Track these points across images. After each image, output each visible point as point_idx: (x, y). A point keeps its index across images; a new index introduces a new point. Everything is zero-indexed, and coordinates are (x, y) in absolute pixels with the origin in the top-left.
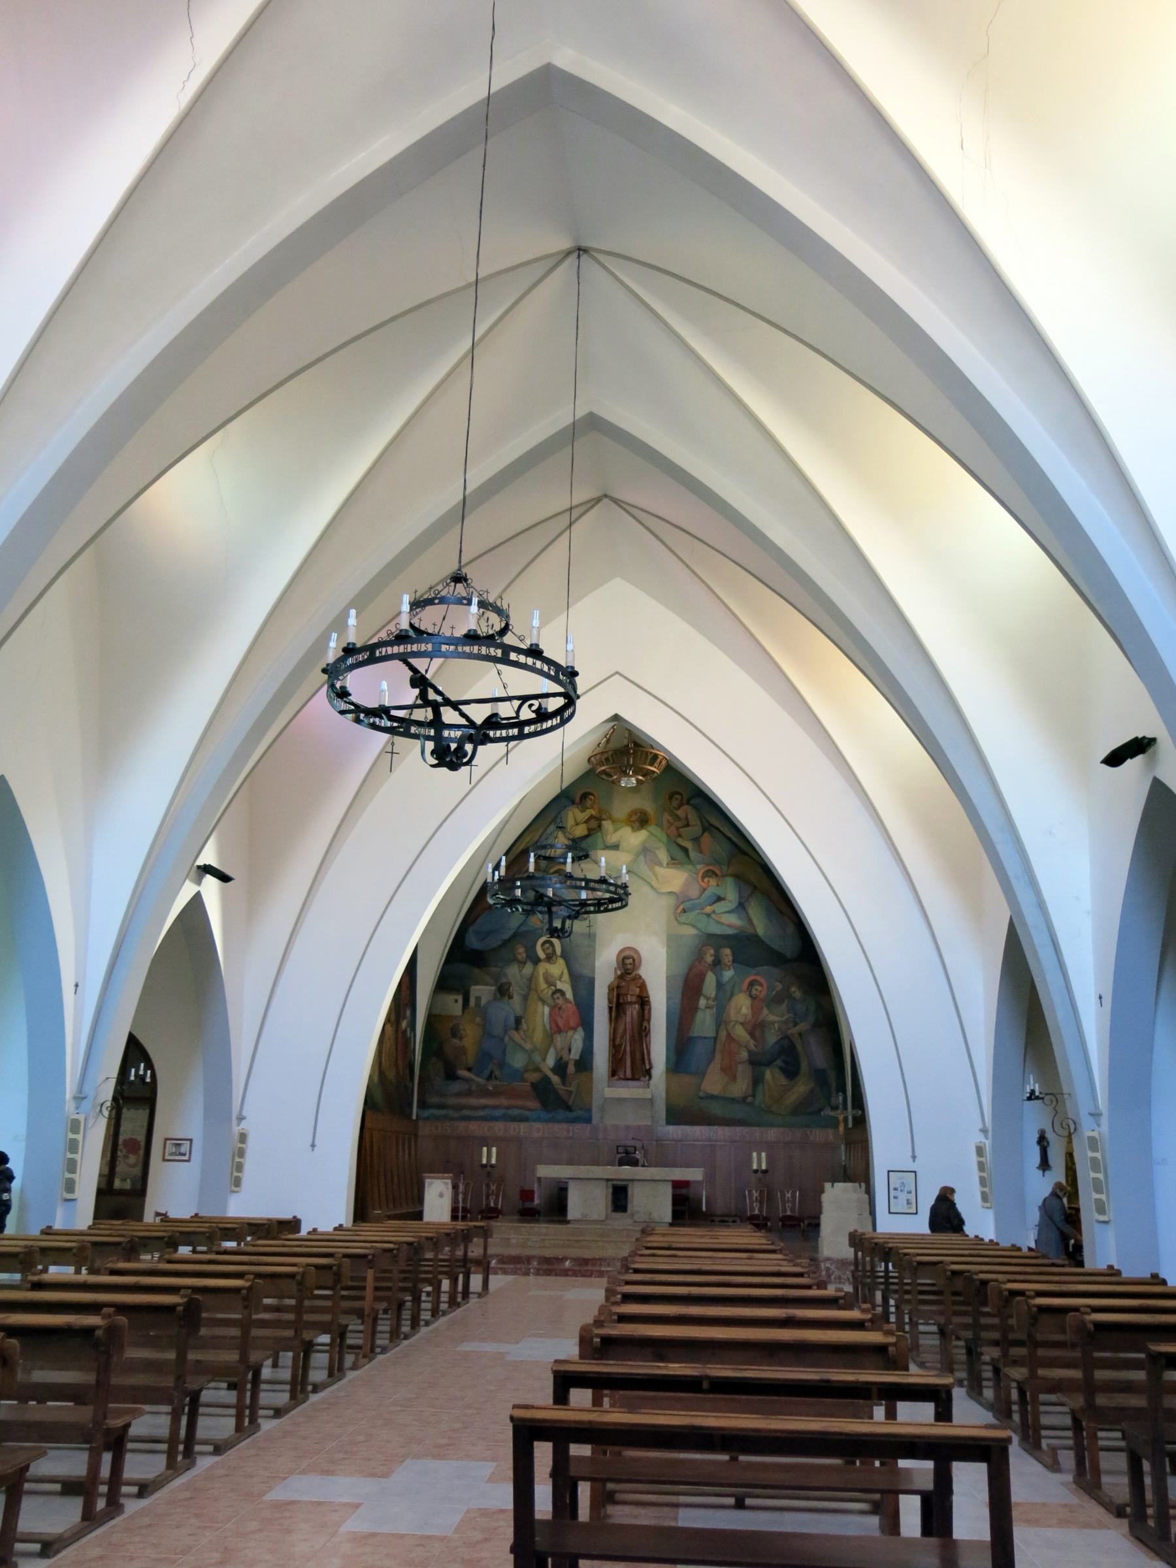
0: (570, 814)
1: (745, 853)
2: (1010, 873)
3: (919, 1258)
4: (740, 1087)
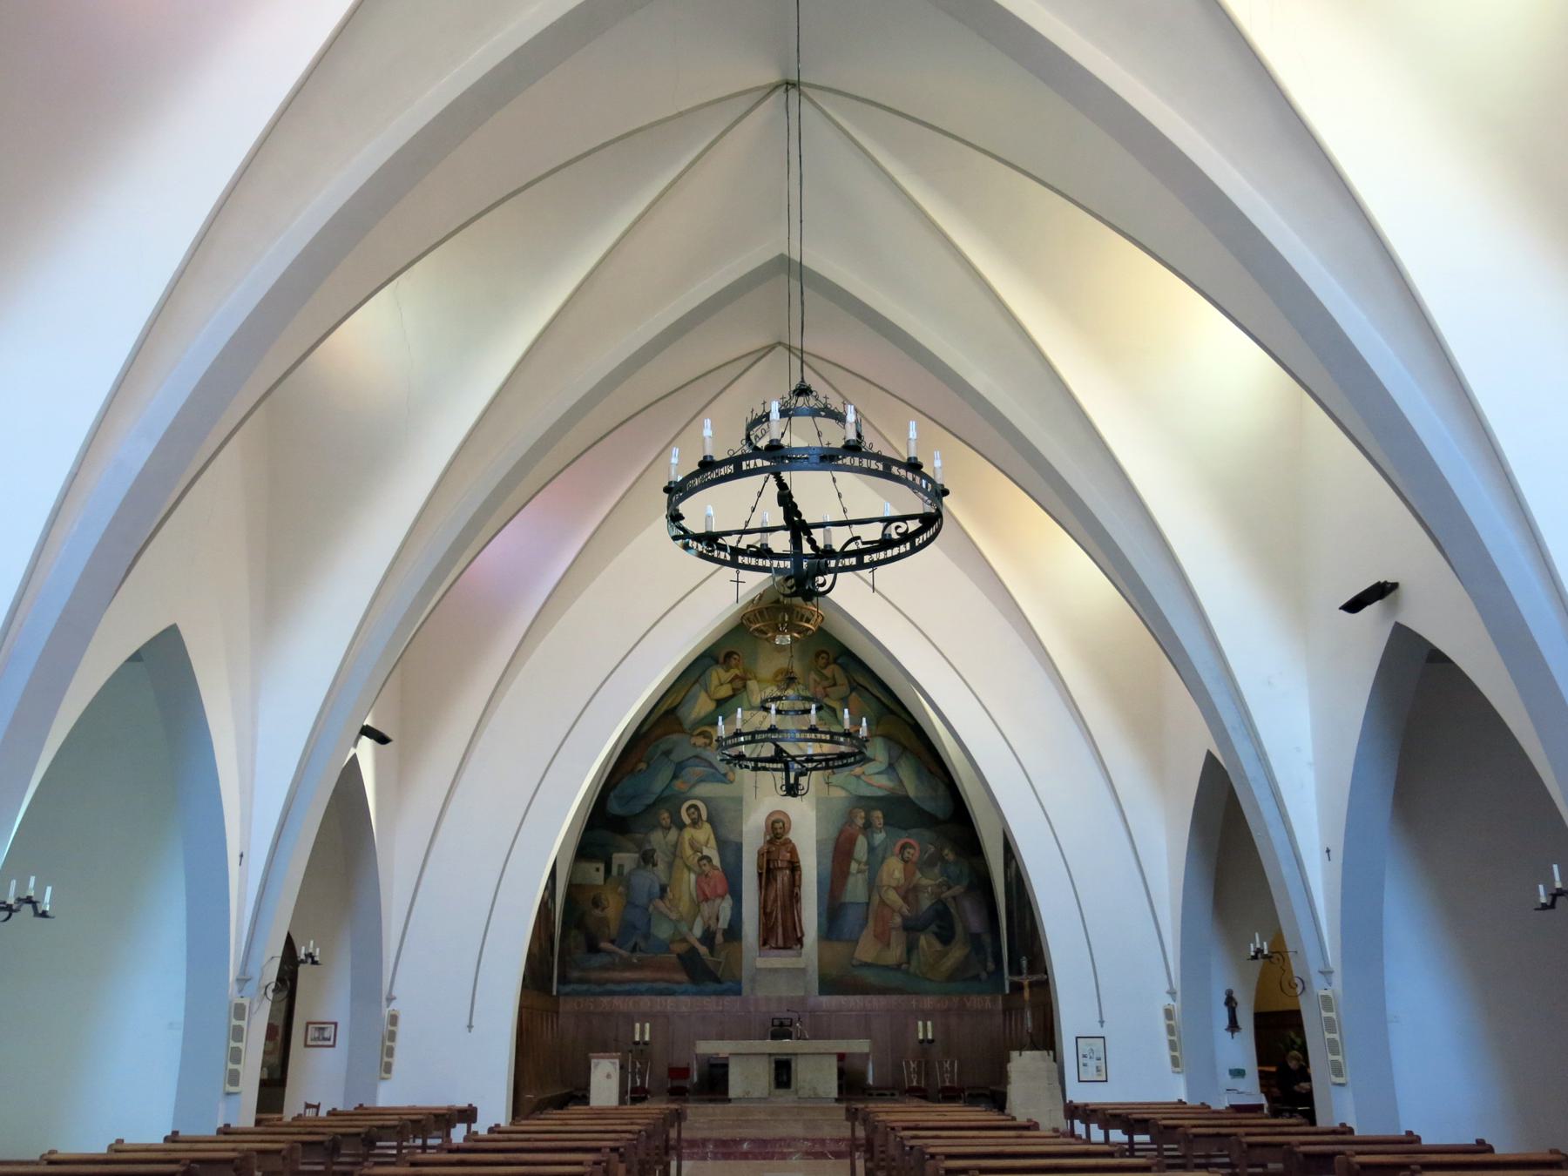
0: (714, 675)
1: (892, 712)
2: (1228, 725)
3: (1195, 1130)
4: (895, 953)
